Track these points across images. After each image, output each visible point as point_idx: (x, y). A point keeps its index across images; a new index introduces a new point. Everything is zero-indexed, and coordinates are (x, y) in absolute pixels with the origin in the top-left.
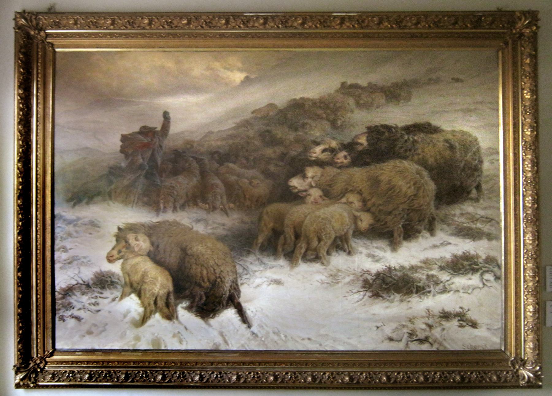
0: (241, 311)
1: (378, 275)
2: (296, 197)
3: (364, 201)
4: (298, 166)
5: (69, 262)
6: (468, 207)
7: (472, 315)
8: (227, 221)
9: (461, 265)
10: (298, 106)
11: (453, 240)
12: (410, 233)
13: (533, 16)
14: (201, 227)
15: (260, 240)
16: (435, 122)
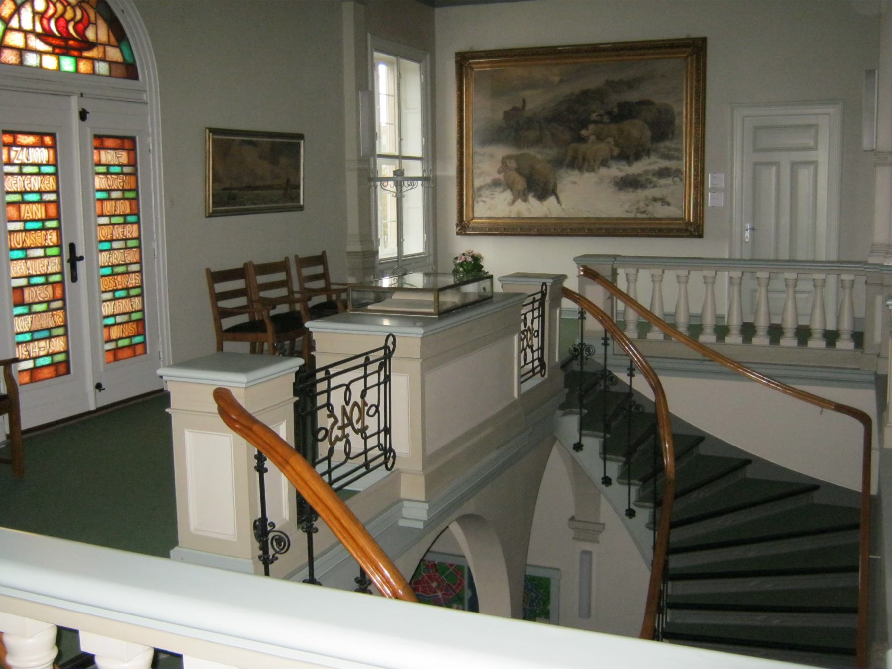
0: (557, 198)
1: (622, 179)
2: (582, 140)
3: (616, 141)
4: (584, 124)
5: (481, 174)
6: (668, 143)
7: (668, 199)
8: (552, 152)
9: (663, 173)
10: (585, 93)
11: (660, 160)
12: (638, 157)
13: (704, 40)
14: (540, 155)
15: (567, 161)
16: (653, 98)
